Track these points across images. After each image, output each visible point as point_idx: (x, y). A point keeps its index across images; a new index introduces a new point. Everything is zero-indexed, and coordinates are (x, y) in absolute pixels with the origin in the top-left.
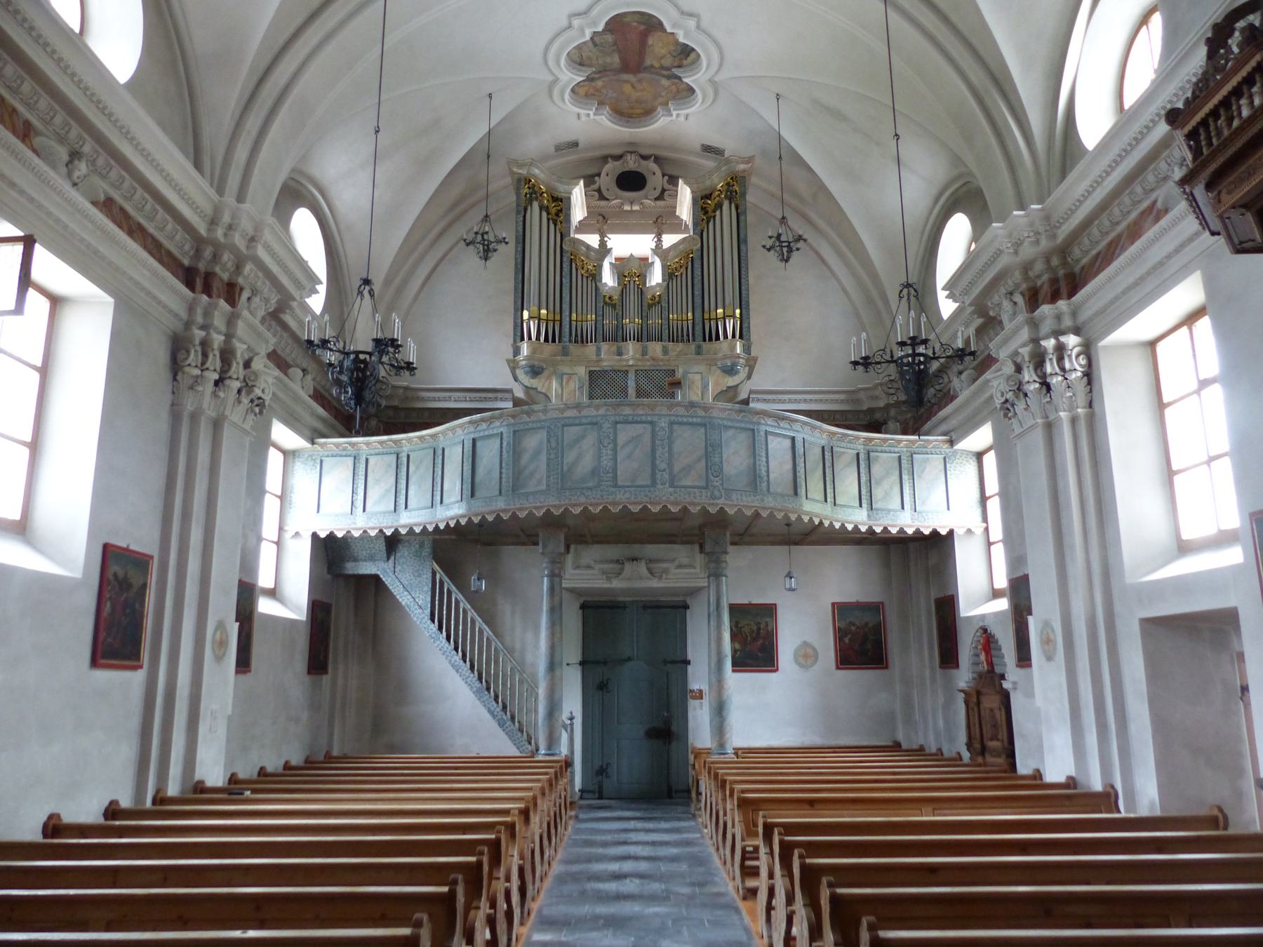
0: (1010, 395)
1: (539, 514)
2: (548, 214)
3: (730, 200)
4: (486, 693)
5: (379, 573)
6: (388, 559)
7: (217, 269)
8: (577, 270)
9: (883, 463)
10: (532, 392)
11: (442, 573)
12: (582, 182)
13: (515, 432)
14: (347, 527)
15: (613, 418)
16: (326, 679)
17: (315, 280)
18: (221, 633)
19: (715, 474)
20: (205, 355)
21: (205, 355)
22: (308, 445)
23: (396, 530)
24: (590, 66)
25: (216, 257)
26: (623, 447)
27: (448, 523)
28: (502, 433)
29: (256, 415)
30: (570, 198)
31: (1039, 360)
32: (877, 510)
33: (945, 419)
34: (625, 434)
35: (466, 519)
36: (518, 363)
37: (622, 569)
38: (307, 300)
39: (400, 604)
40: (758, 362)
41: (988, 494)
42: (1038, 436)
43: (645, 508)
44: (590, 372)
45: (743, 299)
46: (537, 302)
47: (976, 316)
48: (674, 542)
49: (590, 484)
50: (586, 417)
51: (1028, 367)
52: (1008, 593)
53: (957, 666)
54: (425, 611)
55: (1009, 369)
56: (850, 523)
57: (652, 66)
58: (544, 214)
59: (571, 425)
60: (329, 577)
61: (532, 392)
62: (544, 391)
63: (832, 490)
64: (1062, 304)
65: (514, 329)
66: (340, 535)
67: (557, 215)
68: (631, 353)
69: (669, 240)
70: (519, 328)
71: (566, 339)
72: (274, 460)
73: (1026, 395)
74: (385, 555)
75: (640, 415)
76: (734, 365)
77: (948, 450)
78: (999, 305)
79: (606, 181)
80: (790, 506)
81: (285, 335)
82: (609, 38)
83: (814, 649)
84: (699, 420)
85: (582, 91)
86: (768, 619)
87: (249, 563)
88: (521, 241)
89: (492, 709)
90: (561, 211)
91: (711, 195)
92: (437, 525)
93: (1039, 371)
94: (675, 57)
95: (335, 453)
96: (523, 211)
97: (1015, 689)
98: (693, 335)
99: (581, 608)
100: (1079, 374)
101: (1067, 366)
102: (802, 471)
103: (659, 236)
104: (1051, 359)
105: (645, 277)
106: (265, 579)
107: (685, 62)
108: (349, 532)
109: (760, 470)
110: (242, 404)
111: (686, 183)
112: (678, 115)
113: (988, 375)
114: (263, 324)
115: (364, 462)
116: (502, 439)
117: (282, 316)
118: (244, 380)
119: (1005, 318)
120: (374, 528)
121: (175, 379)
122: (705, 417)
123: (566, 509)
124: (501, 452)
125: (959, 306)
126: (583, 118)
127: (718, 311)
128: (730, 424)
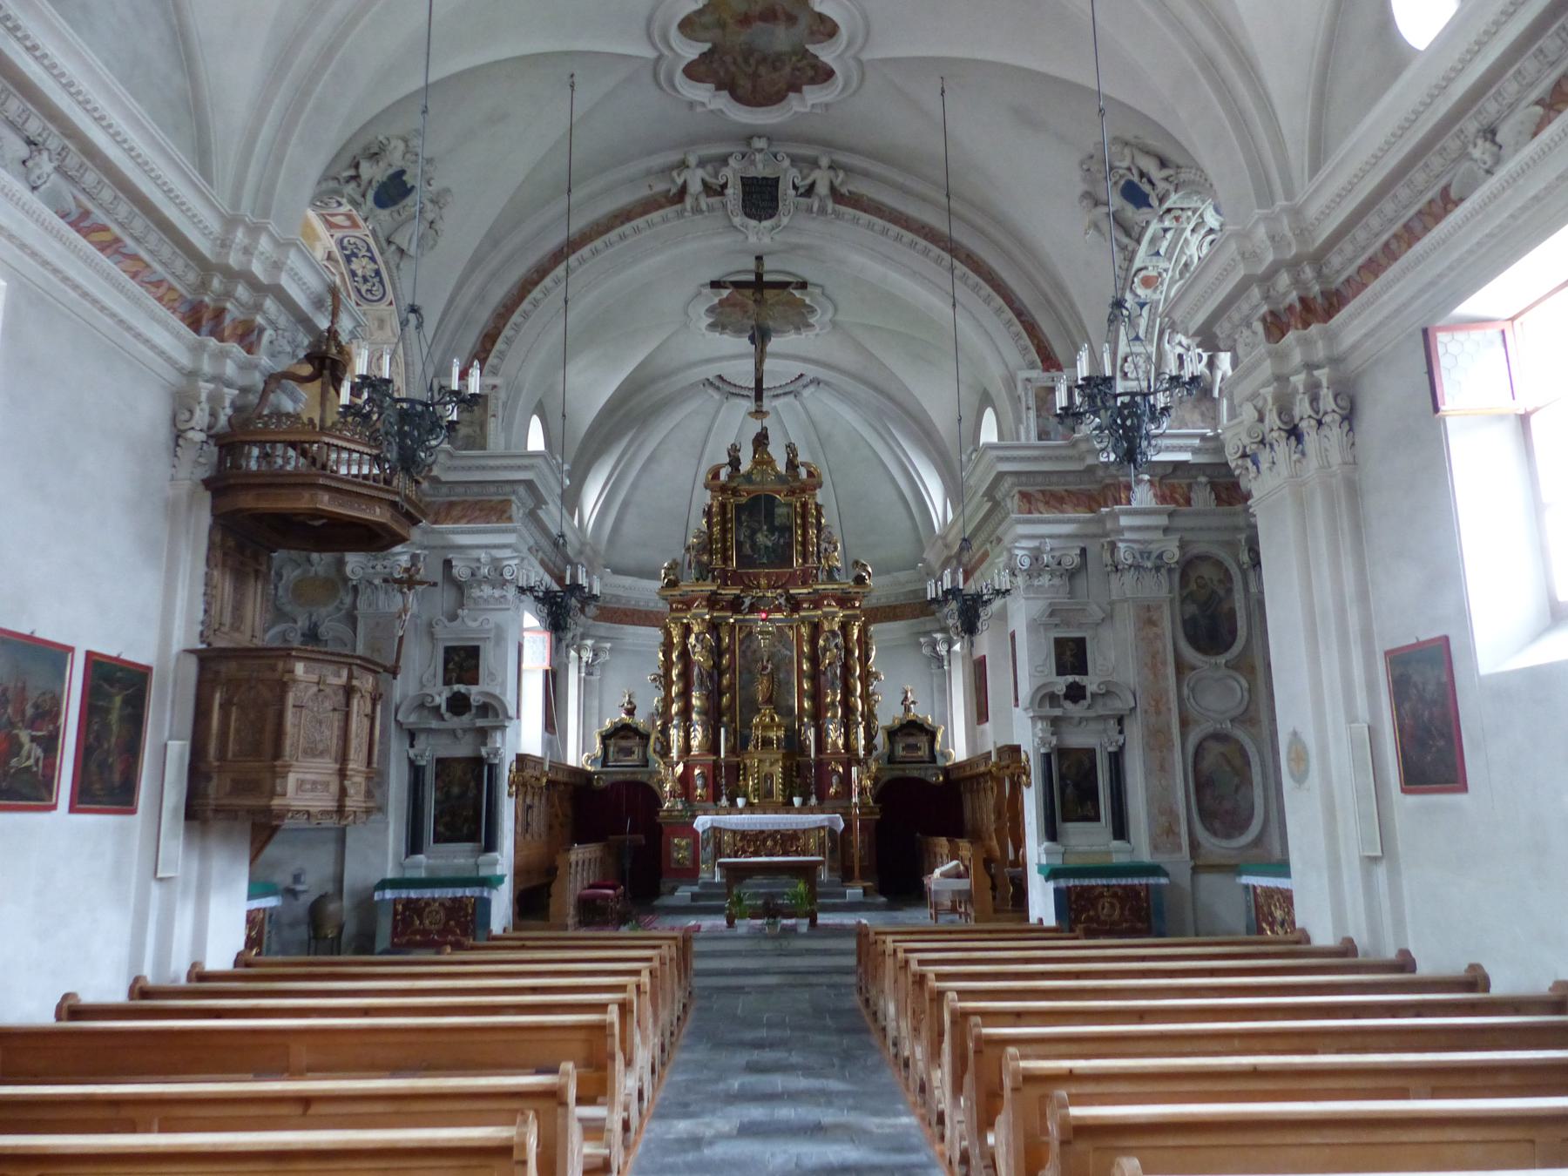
64: (1314, 328)
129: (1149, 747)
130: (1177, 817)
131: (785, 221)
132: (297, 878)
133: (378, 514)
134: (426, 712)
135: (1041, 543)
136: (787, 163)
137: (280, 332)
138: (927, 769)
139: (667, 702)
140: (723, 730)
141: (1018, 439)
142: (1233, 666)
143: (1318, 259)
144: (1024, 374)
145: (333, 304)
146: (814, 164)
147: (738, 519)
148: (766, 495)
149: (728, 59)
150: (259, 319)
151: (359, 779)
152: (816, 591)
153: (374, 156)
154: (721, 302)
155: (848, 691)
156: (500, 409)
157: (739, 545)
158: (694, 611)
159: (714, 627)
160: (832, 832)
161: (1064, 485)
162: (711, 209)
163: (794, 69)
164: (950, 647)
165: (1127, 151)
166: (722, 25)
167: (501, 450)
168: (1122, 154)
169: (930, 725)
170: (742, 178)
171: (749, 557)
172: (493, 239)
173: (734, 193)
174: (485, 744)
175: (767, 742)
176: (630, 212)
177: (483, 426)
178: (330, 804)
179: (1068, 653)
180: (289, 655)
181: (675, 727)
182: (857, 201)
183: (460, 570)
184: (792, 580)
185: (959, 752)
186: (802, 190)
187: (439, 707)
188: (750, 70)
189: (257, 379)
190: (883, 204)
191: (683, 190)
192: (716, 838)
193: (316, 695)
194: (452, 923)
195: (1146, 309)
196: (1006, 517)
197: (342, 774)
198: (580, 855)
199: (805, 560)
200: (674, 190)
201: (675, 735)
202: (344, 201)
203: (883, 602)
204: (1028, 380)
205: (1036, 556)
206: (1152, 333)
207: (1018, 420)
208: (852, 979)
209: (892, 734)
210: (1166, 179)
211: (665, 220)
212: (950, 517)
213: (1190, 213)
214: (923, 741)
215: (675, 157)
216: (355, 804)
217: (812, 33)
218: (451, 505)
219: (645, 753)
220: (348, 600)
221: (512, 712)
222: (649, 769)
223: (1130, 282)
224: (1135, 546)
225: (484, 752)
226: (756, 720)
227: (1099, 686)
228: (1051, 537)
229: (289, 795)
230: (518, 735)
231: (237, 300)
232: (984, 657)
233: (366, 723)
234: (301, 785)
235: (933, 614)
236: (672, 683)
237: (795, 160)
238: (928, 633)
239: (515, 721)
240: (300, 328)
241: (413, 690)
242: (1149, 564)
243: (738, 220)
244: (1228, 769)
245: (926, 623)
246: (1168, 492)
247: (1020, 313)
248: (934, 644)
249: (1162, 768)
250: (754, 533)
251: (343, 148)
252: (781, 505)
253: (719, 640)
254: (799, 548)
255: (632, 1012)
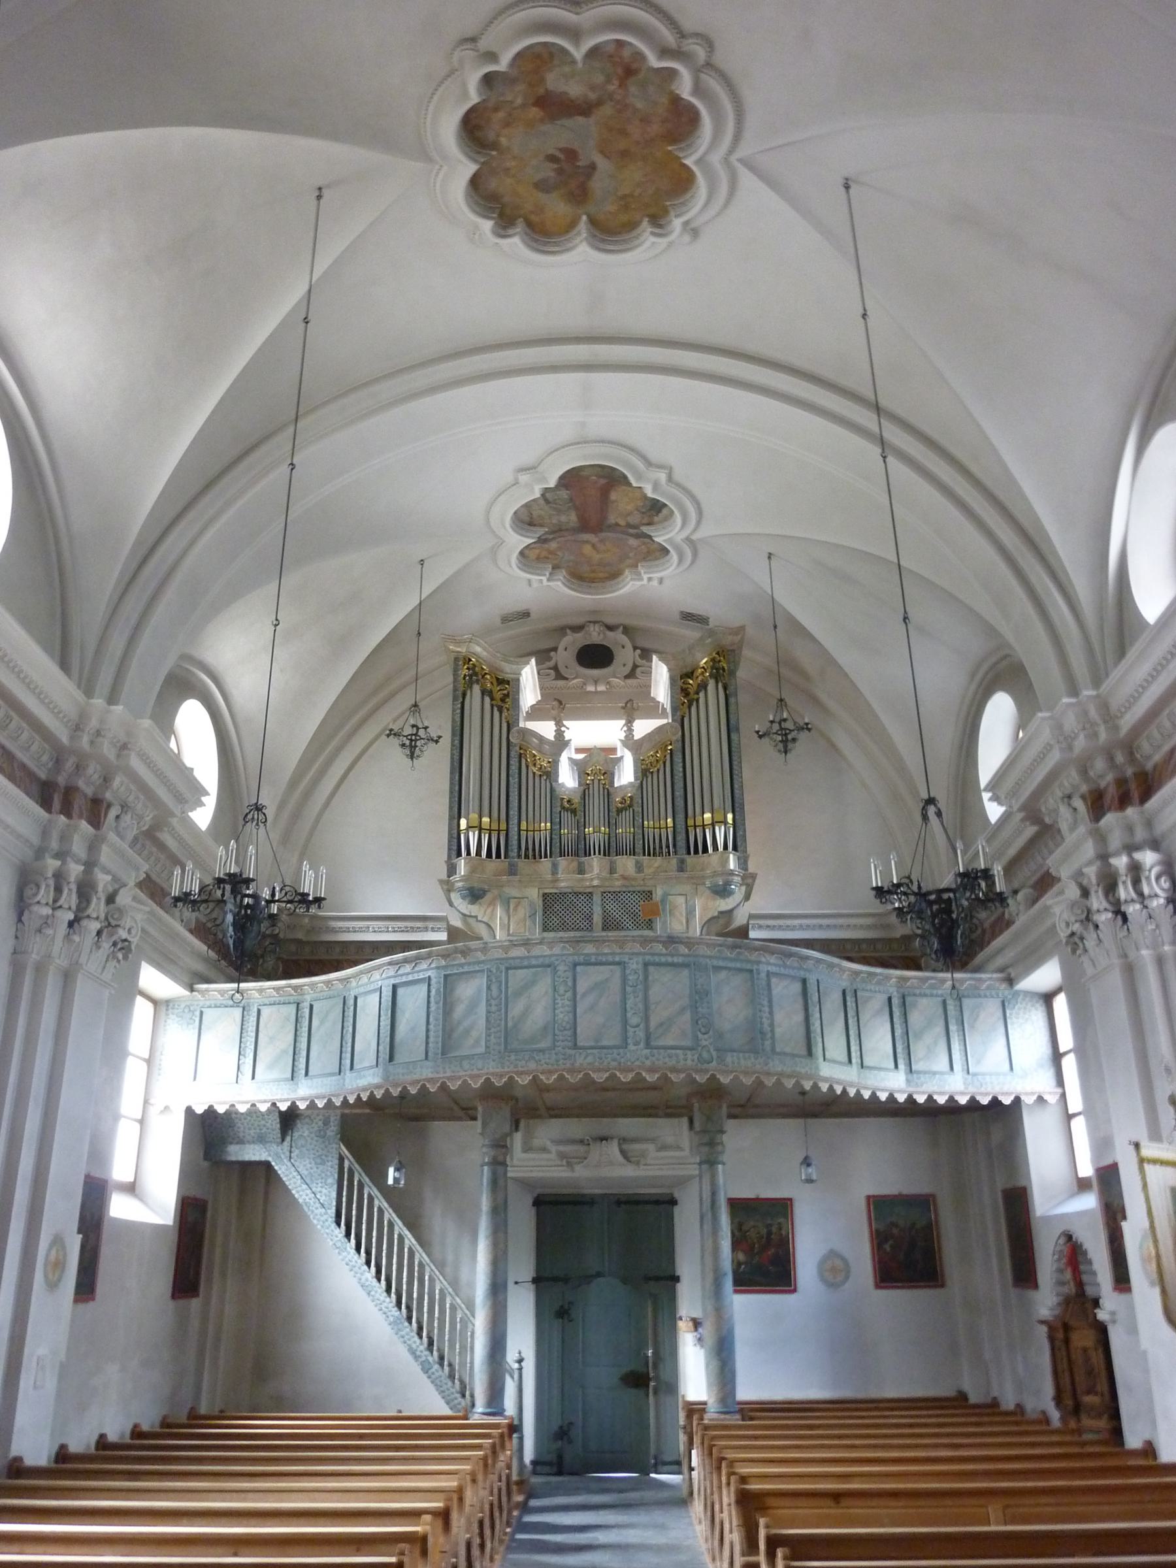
0: (1076, 927)
1: (476, 1085)
2: (492, 699)
3: (716, 677)
4: (406, 1324)
5: (270, 1159)
6: (283, 1140)
7: (81, 784)
8: (527, 767)
9: (923, 1010)
10: (471, 920)
11: (352, 1160)
12: (533, 661)
13: (446, 976)
14: (232, 1099)
15: (571, 959)
16: (195, 1303)
17: (201, 791)
18: (57, 1251)
19: (703, 1030)
20: (58, 890)
21: (58, 890)
22: (186, 993)
23: (294, 1103)
24: (541, 526)
25: (79, 768)
26: (584, 995)
27: (359, 1095)
28: (429, 977)
29: (119, 961)
30: (518, 680)
31: (1110, 885)
32: (918, 1072)
33: (1000, 951)
34: (588, 978)
35: (382, 1091)
36: (453, 884)
37: (588, 1152)
38: (190, 814)
39: (295, 1200)
40: (757, 881)
41: (1062, 1050)
42: (1116, 979)
43: (613, 1076)
44: (544, 895)
45: (736, 800)
46: (477, 808)
47: (1028, 823)
48: (656, 1116)
49: (542, 1045)
50: (537, 957)
51: (1097, 892)
52: (1095, 1183)
53: (1035, 1286)
54: (329, 1211)
55: (1073, 892)
56: (883, 1090)
57: (617, 525)
58: (487, 700)
59: (516, 968)
60: (206, 1164)
61: (471, 920)
62: (485, 919)
63: (858, 1048)
64: (1130, 811)
65: (449, 841)
66: (221, 1109)
67: (503, 700)
68: (596, 871)
69: (643, 727)
70: (456, 840)
71: (514, 853)
72: (142, 1010)
73: (1097, 927)
74: (279, 1135)
75: (606, 954)
76: (727, 883)
77: (1007, 992)
78: (1056, 811)
79: (565, 656)
80: (803, 1071)
81: (162, 857)
82: (564, 494)
83: (843, 1259)
84: (680, 960)
85: (532, 554)
86: (781, 1220)
87: (99, 1152)
88: (458, 733)
89: (414, 1346)
90: (507, 695)
91: (692, 673)
92: (345, 1098)
93: (1111, 898)
94: (643, 513)
95: (218, 1003)
96: (460, 698)
97: (1114, 1322)
98: (675, 846)
99: (534, 1205)
100: (1162, 901)
101: (1146, 891)
102: (818, 1023)
103: (629, 723)
104: (1124, 883)
105: (613, 775)
106: (120, 1170)
107: (656, 519)
108: (233, 1106)
109: (762, 1023)
110: (102, 949)
111: (661, 659)
112: (650, 579)
113: (1048, 899)
114: (131, 848)
115: (255, 1014)
116: (429, 985)
117: (158, 834)
118: (106, 918)
119: (1064, 826)
120: (265, 1101)
121: (20, 920)
122: (688, 956)
123: (511, 1078)
124: (429, 1002)
125: (1006, 811)
126: (535, 585)
127: (705, 816)
128: (721, 963)
143: (1129, 746)
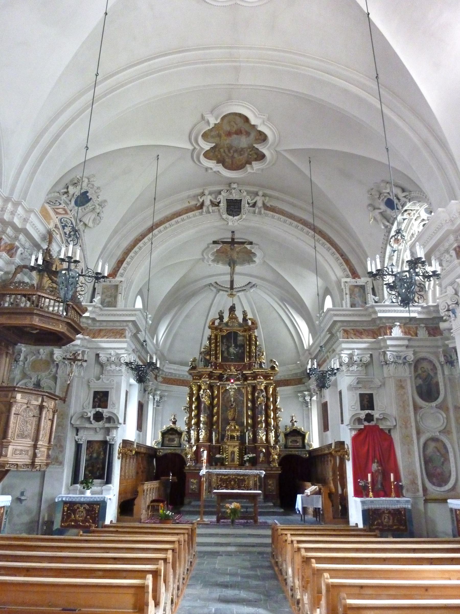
129: (403, 443)
130: (417, 475)
131: (244, 217)
132: (22, 494)
133: (61, 328)
134: (84, 420)
135: (353, 352)
136: (245, 194)
137: (26, 250)
138: (301, 451)
139: (190, 418)
140: (214, 433)
141: (342, 307)
142: (439, 407)
144: (344, 280)
145: (50, 238)
146: (257, 194)
147: (222, 342)
148: (234, 332)
149: (222, 150)
150: (17, 244)
151: (44, 450)
152: (254, 372)
153: (75, 184)
154: (217, 251)
155: (267, 416)
156: (123, 291)
157: (222, 352)
158: (203, 380)
159: (211, 387)
160: (260, 478)
161: (362, 327)
162: (213, 212)
163: (249, 154)
164: (311, 398)
165: (388, 185)
166: (219, 136)
167: (123, 308)
168: (386, 187)
169: (303, 432)
170: (227, 199)
171: (227, 357)
172: (124, 222)
173: (223, 205)
174: (108, 435)
175: (232, 437)
176: (180, 213)
177: (115, 297)
178: (27, 460)
179: (366, 400)
180: (14, 390)
181: (193, 430)
182: (274, 209)
183: (103, 358)
184: (244, 368)
185: (315, 444)
186: (251, 205)
187: (90, 418)
188: (230, 155)
189: (13, 268)
190: (284, 210)
191: (202, 205)
192: (209, 479)
193: (25, 409)
194: (88, 517)
195: (396, 252)
196: (336, 341)
197: (35, 447)
198: (149, 486)
199: (250, 359)
200: (199, 204)
201: (193, 434)
202: (62, 202)
203: (283, 378)
204: (346, 282)
205: (351, 357)
206: (399, 263)
207: (342, 299)
208: (269, 550)
209: (286, 435)
210: (405, 197)
211: (195, 216)
212: (311, 342)
213: (415, 212)
214: (299, 439)
215: (199, 191)
216: (40, 461)
217: (256, 140)
218: (100, 330)
219: (180, 441)
220: (54, 370)
221: (121, 421)
222: (182, 448)
223: (389, 241)
224: (394, 353)
225: (108, 438)
226: (228, 427)
227: (380, 415)
228: (357, 349)
229: (8, 456)
230: (124, 431)
231: (6, 234)
232: (327, 402)
233: (49, 423)
234: (15, 452)
235: (304, 384)
236: (192, 410)
237: (248, 193)
238: (302, 392)
239: (123, 425)
240: (35, 248)
241: (79, 410)
242: (400, 361)
243: (225, 216)
244: (438, 454)
245: (301, 387)
246: (407, 330)
247: (342, 255)
248: (304, 396)
249: (409, 453)
250: (228, 347)
251: (61, 179)
252: (240, 336)
253: (213, 392)
254: (248, 354)
255: (161, 576)
